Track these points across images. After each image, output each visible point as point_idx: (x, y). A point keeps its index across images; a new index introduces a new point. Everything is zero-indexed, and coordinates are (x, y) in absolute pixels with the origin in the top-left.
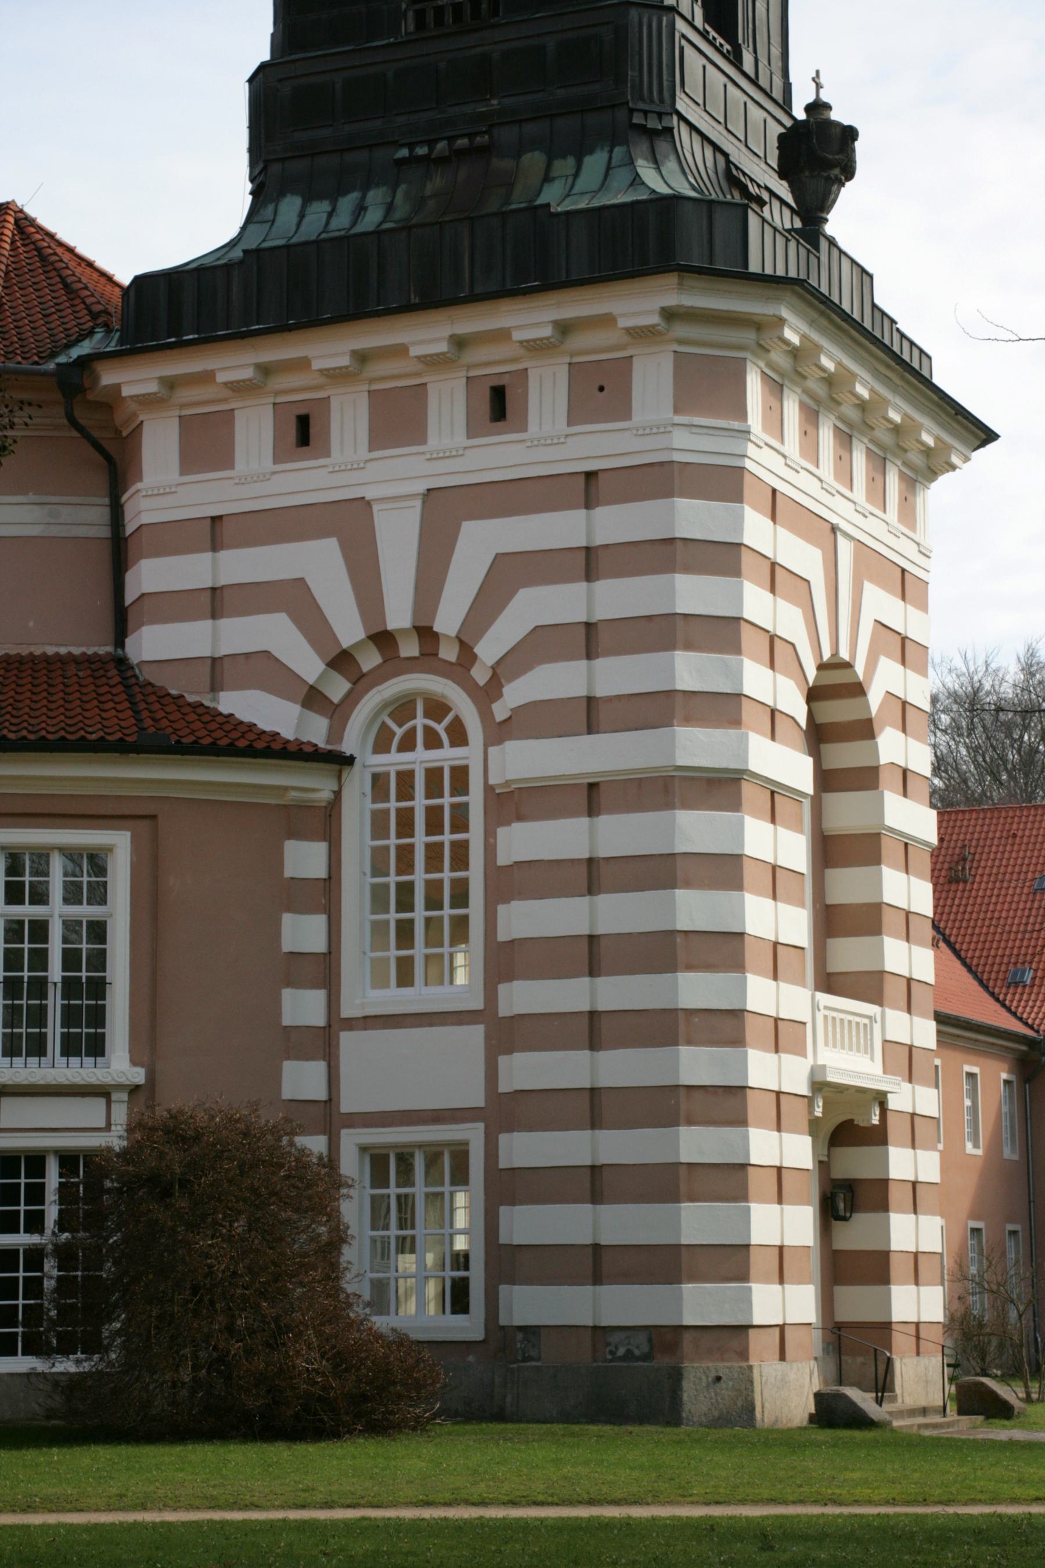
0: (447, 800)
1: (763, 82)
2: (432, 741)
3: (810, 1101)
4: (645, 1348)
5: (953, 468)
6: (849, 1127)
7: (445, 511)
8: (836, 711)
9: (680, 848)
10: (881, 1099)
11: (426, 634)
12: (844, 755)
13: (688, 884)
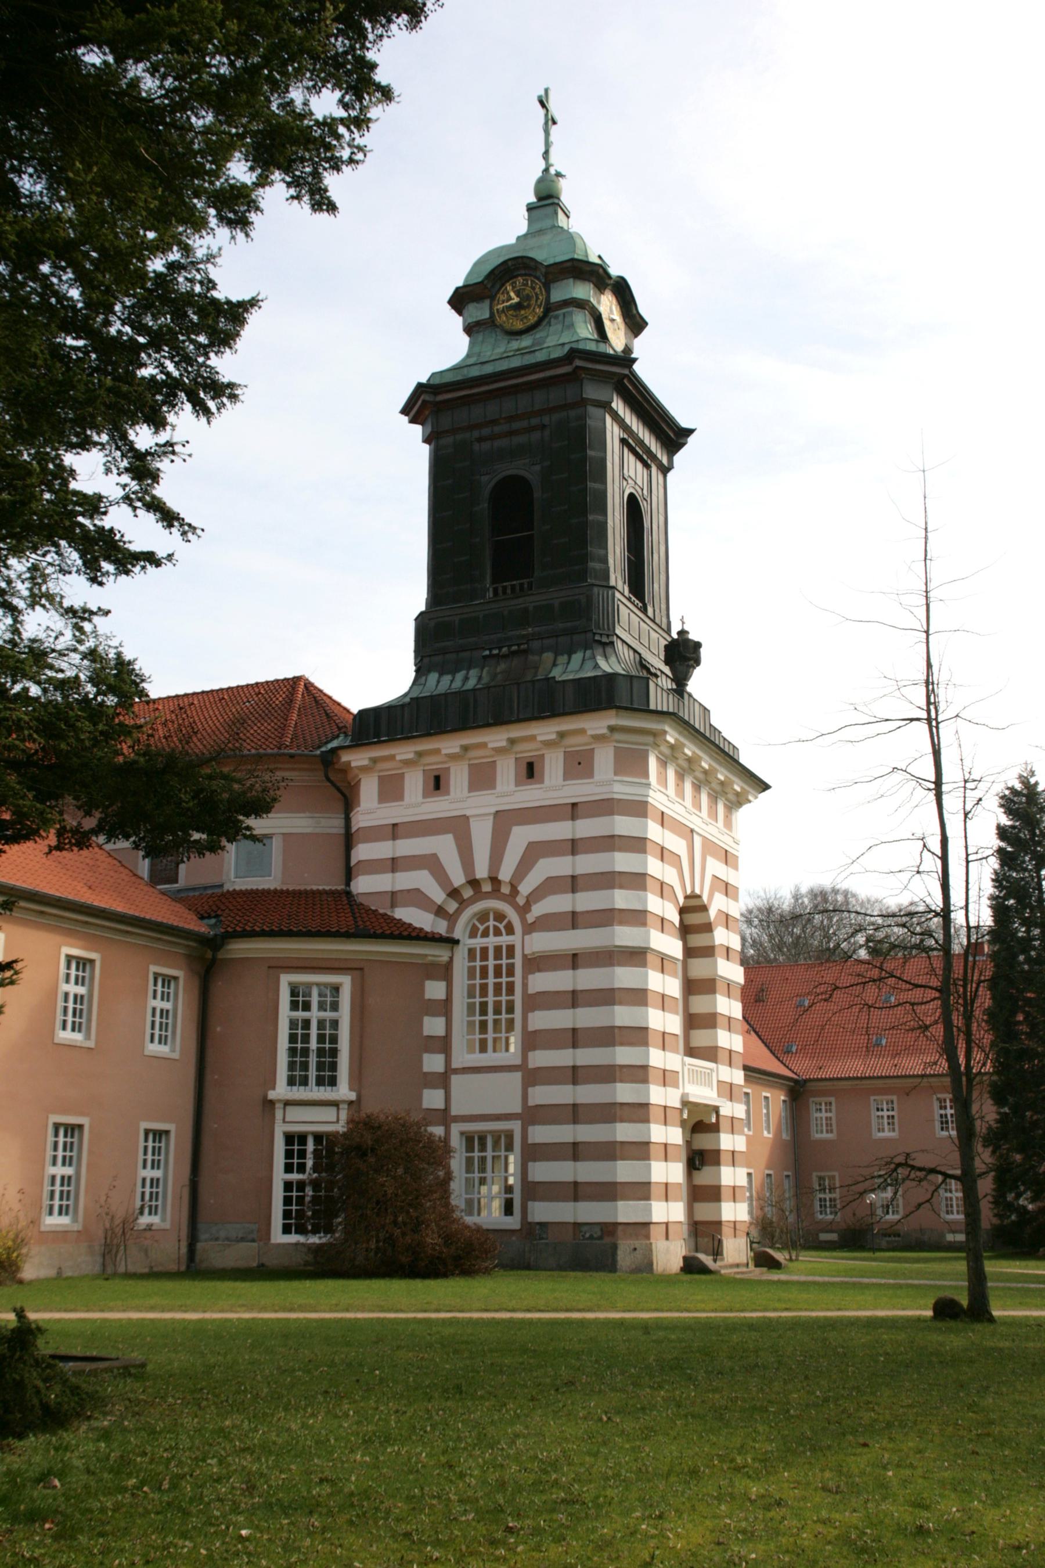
0: (504, 962)
1: (657, 620)
2: (497, 933)
3: (681, 1111)
4: (599, 1233)
5: (750, 802)
6: (701, 1124)
7: (504, 822)
8: (694, 919)
9: (616, 986)
10: (716, 1109)
11: (495, 880)
12: (697, 940)
13: (621, 1003)
